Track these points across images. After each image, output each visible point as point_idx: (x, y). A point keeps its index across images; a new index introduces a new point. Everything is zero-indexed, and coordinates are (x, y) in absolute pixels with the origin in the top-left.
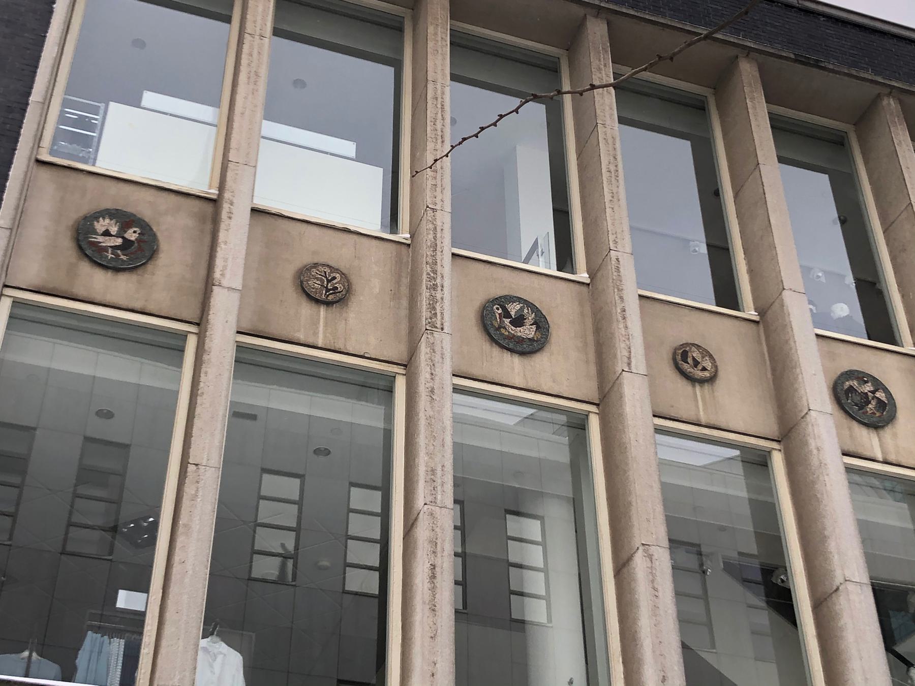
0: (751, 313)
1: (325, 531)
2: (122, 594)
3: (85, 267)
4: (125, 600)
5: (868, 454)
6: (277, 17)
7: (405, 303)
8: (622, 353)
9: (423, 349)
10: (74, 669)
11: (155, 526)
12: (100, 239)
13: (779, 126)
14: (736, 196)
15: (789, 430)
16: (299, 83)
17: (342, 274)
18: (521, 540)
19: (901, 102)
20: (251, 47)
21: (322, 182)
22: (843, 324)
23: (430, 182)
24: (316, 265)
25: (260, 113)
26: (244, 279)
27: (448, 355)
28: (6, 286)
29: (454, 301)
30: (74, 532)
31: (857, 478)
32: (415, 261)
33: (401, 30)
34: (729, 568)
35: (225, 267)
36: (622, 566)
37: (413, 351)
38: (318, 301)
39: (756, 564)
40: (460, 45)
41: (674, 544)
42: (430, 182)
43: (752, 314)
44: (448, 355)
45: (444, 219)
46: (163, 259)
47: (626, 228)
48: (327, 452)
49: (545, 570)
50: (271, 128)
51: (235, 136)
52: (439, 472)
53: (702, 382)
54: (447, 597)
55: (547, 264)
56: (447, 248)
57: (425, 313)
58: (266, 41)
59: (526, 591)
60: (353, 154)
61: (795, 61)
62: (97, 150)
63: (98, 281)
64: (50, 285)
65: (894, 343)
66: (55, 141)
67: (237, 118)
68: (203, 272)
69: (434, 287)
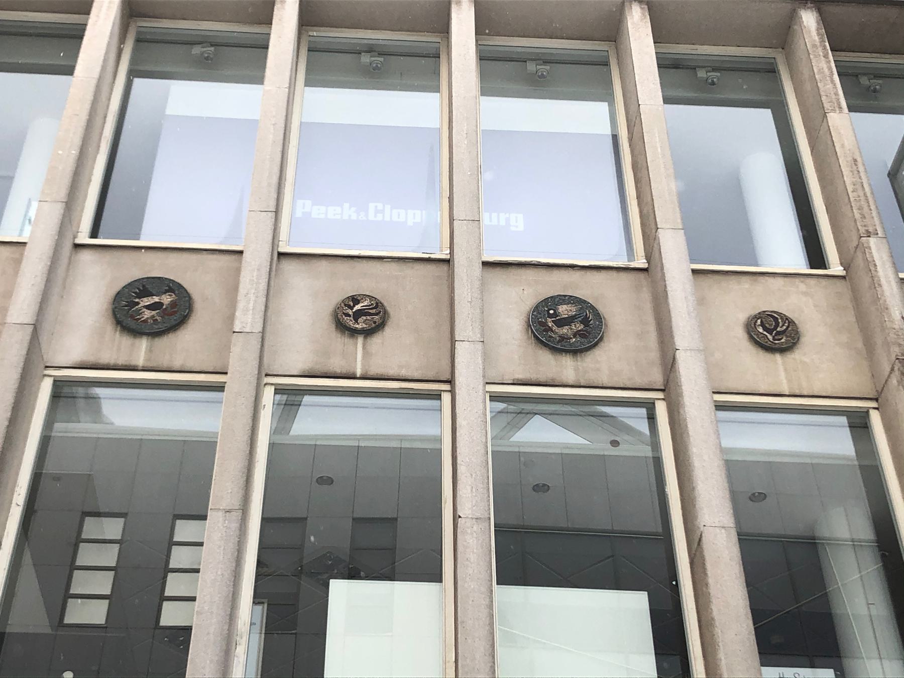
0: (836, 269)
19: (820, 12)
31: (501, 406)
33: (606, 64)
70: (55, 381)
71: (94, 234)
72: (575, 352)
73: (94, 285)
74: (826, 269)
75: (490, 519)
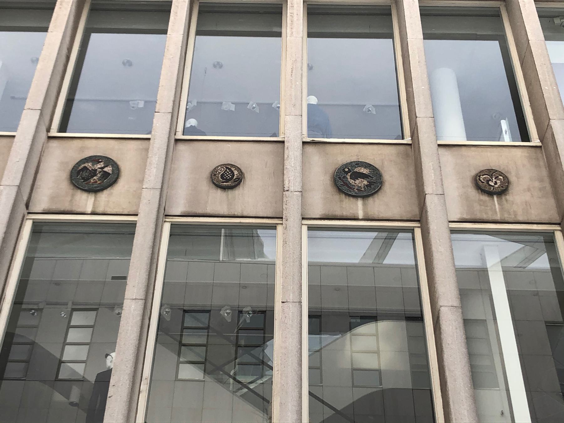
0: (535, 141)
33: (390, 15)
70: (33, 222)
71: (63, 128)
72: (365, 197)
73: (59, 161)
74: (529, 141)
75: (300, 302)
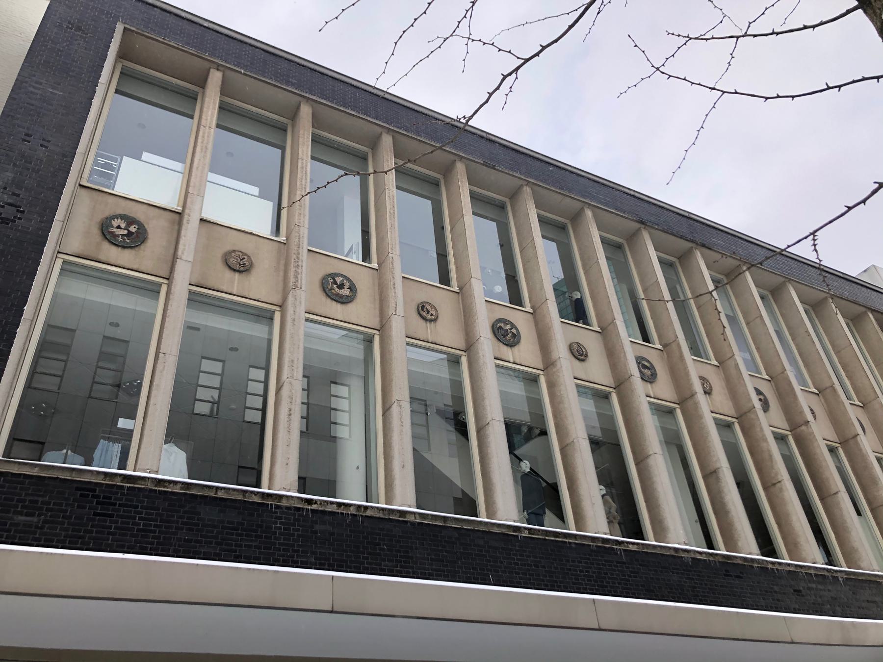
0: (456, 288)
1: (232, 390)
2: (121, 420)
3: (106, 245)
4: (122, 423)
5: (507, 359)
6: (219, 118)
7: (282, 274)
8: (392, 305)
9: (290, 299)
10: (93, 459)
11: (140, 384)
12: (115, 230)
13: (474, 196)
14: (452, 230)
15: (470, 347)
16: (230, 154)
17: (249, 256)
18: (337, 396)
20: (204, 133)
21: (238, 206)
22: (499, 296)
23: (298, 212)
24: (234, 251)
25: (207, 169)
26: (194, 256)
27: (303, 303)
28: (59, 252)
29: (308, 275)
30: (96, 387)
31: (502, 370)
32: (288, 251)
33: (285, 130)
34: (439, 412)
35: (184, 249)
36: (386, 410)
37: (285, 299)
38: (234, 270)
39: (451, 410)
40: (316, 140)
41: (413, 399)
42: (298, 212)
43: (456, 289)
44: (303, 303)
45: (305, 231)
46: (150, 243)
47: (397, 242)
48: (236, 349)
49: (350, 412)
50: (212, 177)
51: (193, 179)
52: (296, 362)
53: (430, 321)
54: (297, 425)
55: (357, 258)
56: (305, 247)
57: (292, 280)
58: (212, 130)
59: (338, 421)
60: (257, 194)
61: (483, 165)
62: (115, 182)
63: (112, 253)
64: (85, 254)
65: (522, 306)
66: (90, 175)
67: (194, 170)
68: (172, 251)
69: (298, 266)
